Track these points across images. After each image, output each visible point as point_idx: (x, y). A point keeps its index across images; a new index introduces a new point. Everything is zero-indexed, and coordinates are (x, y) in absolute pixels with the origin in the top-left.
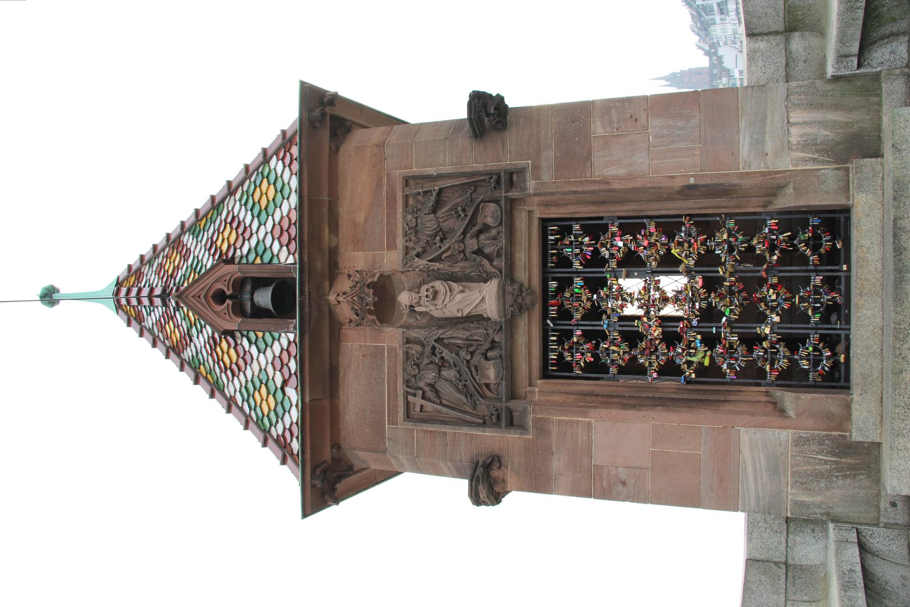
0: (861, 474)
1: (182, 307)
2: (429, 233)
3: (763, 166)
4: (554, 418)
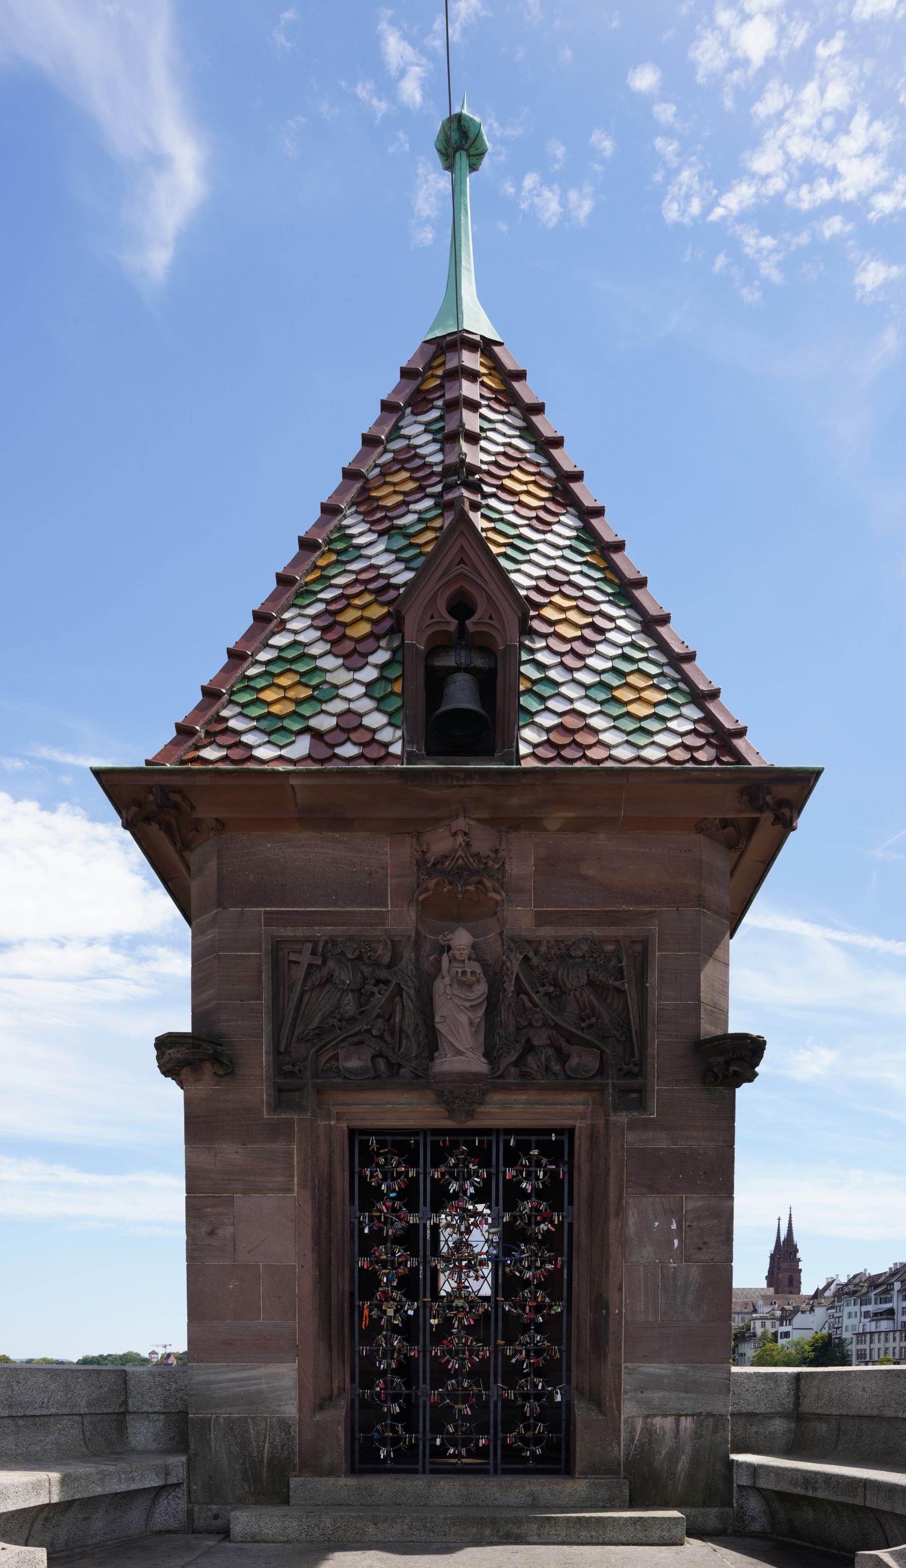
0: (249, 1487)
1: (441, 515)
2: (560, 977)
3: (628, 1387)
4: (295, 1147)
